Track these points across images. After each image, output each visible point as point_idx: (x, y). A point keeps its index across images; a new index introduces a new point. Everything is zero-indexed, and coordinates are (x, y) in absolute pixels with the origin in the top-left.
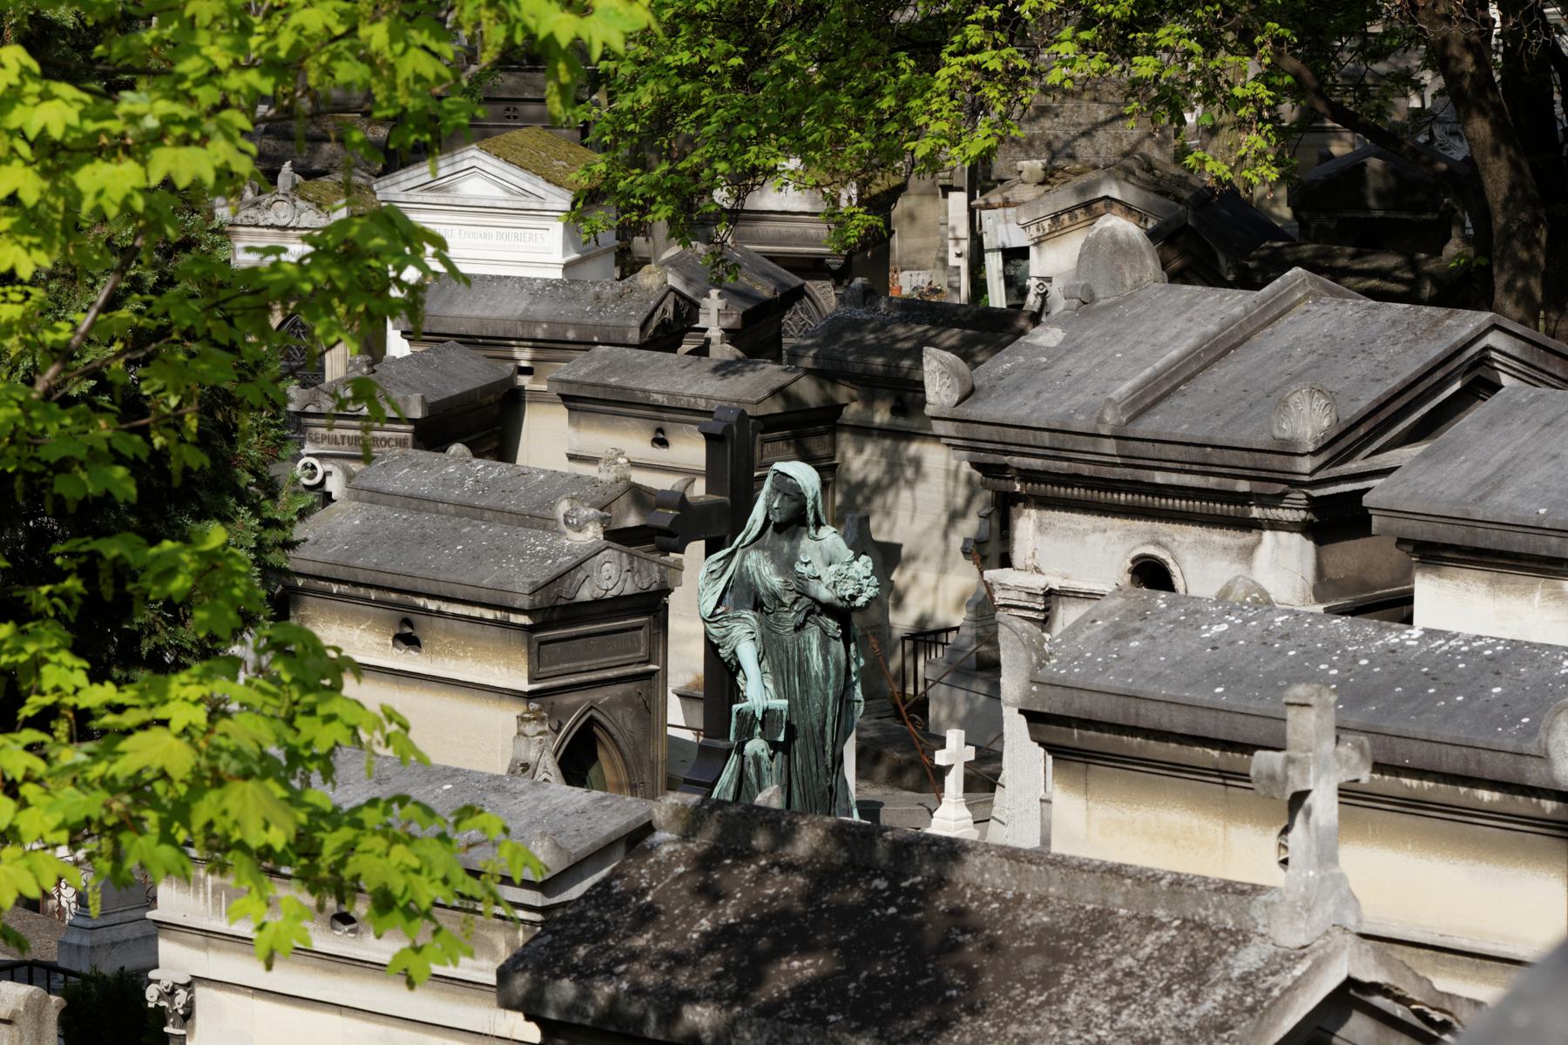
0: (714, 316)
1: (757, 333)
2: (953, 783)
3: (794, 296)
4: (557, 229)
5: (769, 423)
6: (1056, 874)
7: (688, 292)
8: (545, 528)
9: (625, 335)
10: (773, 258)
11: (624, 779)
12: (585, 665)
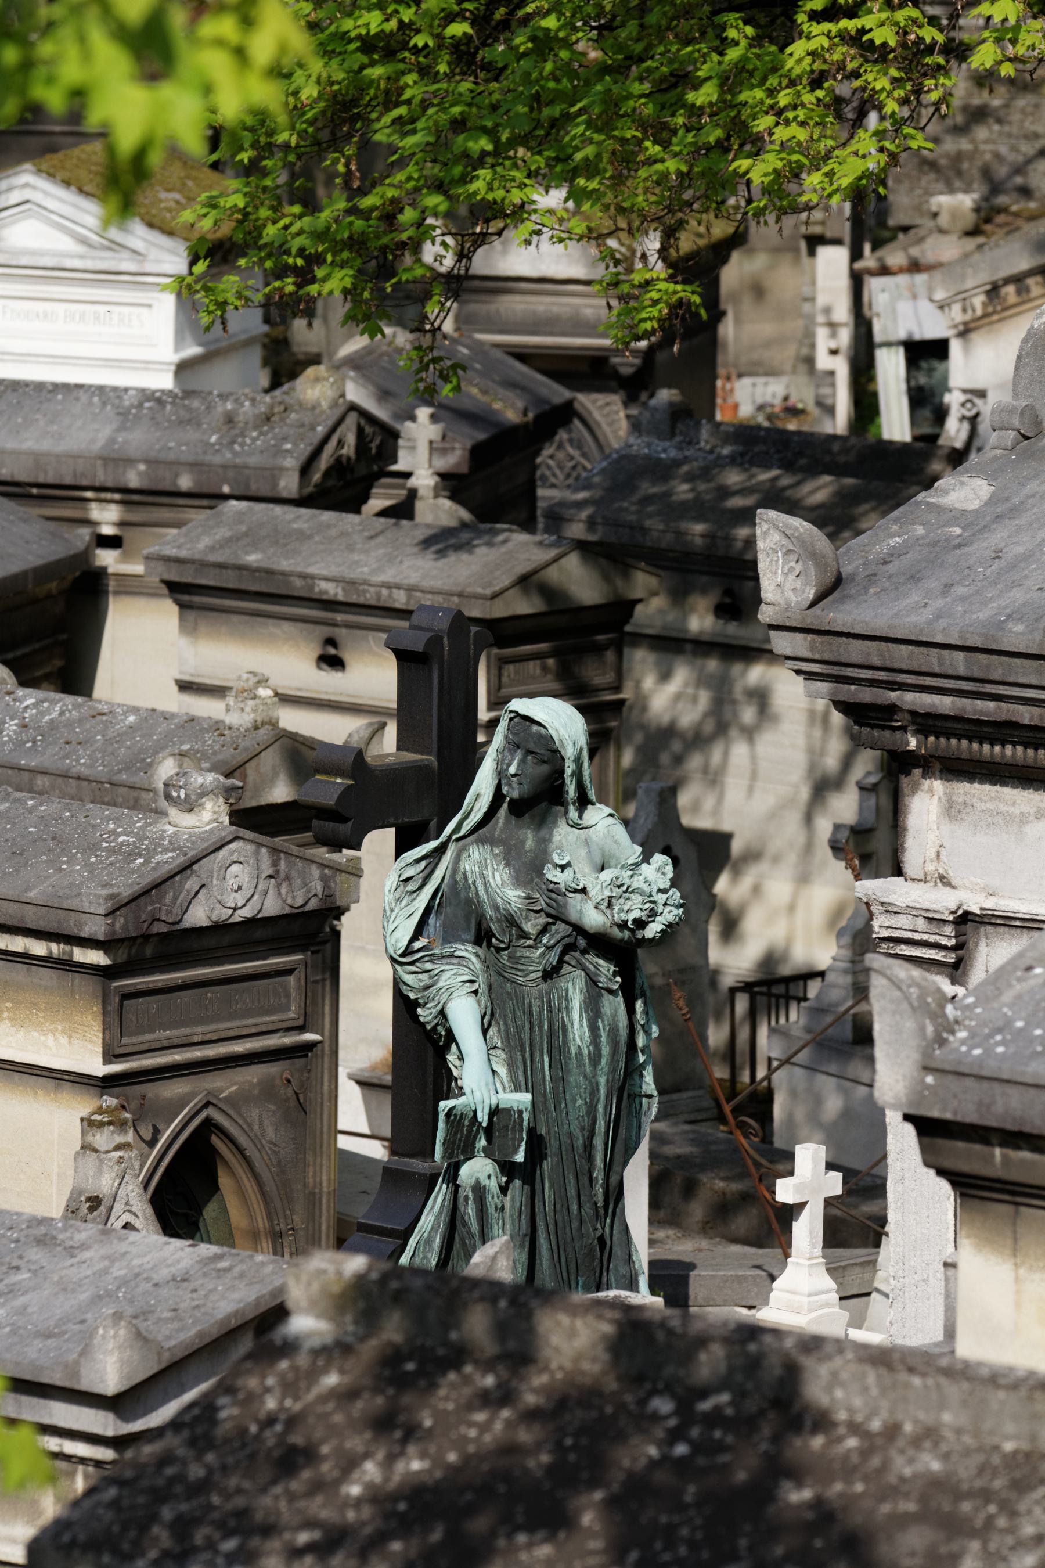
0: (422, 451)
1: (495, 482)
2: (807, 1232)
3: (556, 419)
4: (167, 304)
5: (503, 633)
6: (954, 1391)
7: (381, 413)
8: (135, 806)
9: (274, 481)
10: (523, 355)
11: (262, 1222)
12: (198, 1032)
